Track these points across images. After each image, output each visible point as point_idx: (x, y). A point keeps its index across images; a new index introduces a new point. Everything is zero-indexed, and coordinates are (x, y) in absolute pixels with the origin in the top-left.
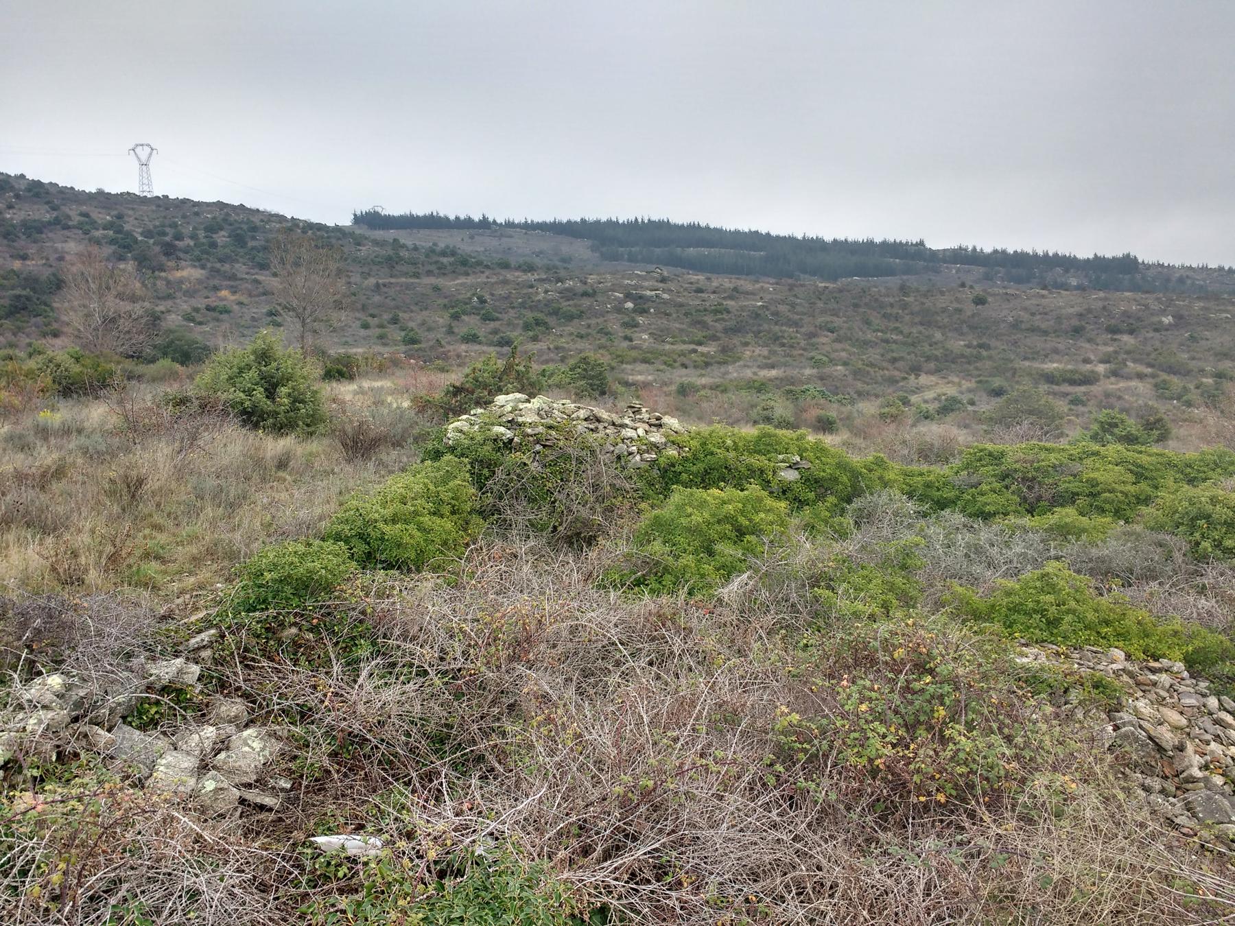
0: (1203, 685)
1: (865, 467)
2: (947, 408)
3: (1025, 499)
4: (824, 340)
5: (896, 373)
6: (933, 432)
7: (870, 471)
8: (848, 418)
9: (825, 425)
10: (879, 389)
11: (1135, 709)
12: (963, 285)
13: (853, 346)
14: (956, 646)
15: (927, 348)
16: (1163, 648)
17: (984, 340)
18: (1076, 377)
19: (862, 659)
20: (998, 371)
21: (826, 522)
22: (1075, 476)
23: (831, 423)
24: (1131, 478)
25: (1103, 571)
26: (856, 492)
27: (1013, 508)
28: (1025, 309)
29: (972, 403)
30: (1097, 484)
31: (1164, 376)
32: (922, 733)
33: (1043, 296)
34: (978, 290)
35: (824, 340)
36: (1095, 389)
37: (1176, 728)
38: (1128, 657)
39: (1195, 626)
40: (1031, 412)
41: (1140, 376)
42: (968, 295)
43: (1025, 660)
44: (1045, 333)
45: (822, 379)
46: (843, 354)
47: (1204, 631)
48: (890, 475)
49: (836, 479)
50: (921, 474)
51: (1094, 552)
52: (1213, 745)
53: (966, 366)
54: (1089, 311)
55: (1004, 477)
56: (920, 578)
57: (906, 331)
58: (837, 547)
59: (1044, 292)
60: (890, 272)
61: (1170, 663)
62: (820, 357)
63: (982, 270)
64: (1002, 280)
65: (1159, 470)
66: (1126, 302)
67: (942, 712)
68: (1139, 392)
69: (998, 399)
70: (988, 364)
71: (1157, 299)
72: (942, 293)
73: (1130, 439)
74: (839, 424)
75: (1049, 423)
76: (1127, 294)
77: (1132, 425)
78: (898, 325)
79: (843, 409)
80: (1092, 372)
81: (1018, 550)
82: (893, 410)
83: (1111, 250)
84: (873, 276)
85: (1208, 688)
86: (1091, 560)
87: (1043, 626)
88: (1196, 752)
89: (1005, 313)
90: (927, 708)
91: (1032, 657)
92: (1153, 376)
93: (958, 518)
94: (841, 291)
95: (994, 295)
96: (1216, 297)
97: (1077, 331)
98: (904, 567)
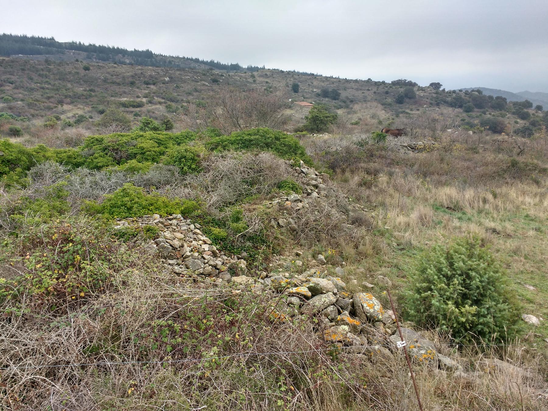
0: (188, 221)
1: (35, 151)
2: (80, 120)
3: (115, 159)
4: (8, 88)
5: (51, 104)
6: (71, 132)
7: (38, 153)
8: (27, 128)
9: (15, 133)
10: (43, 113)
11: (164, 236)
12: (77, 61)
13: (25, 91)
14: (80, 226)
15: (64, 91)
16: (173, 210)
17: (92, 87)
18: (135, 104)
19: (36, 243)
20: (101, 102)
21: (17, 182)
22: (134, 146)
23: (18, 131)
24: (156, 145)
25: (148, 184)
26: (33, 164)
27: (111, 163)
28: (108, 73)
29: (91, 118)
30: (144, 149)
31: (169, 103)
32: (71, 269)
33: (115, 67)
34: (85, 63)
35: (8, 88)
36: (144, 109)
37: (180, 239)
38: (161, 216)
39: (183, 200)
40: (117, 120)
41: (160, 103)
42: (80, 65)
43: (119, 227)
44: (119, 84)
45: (10, 108)
46: (20, 95)
47: (187, 201)
48: (48, 154)
49: (19, 159)
50: (65, 152)
51: (145, 177)
52: (194, 242)
53: (85, 100)
54: (136, 74)
55: (105, 149)
56: (69, 201)
57: (52, 82)
58: (22, 192)
59: (115, 65)
60: (39, 53)
61: (176, 215)
62: (7, 97)
63: (85, 53)
64: (96, 59)
65: (166, 141)
66: (150, 71)
67: (78, 257)
68: (160, 109)
69: (103, 115)
70: (95, 99)
71: (162, 70)
72: (68, 64)
73: (155, 129)
74: (23, 132)
75: (125, 124)
76: (150, 67)
77: (156, 123)
78: (47, 80)
79: (25, 124)
80: (141, 102)
81: (113, 180)
82: (51, 123)
83: (141, 48)
84: (30, 55)
85: (190, 222)
86: (144, 181)
87: (126, 211)
88: (188, 246)
89: (99, 75)
90: (71, 257)
91: (122, 225)
92: (165, 103)
93: (86, 171)
94: (12, 62)
95: (93, 66)
96: (183, 70)
97: (132, 84)
98: (59, 197)
